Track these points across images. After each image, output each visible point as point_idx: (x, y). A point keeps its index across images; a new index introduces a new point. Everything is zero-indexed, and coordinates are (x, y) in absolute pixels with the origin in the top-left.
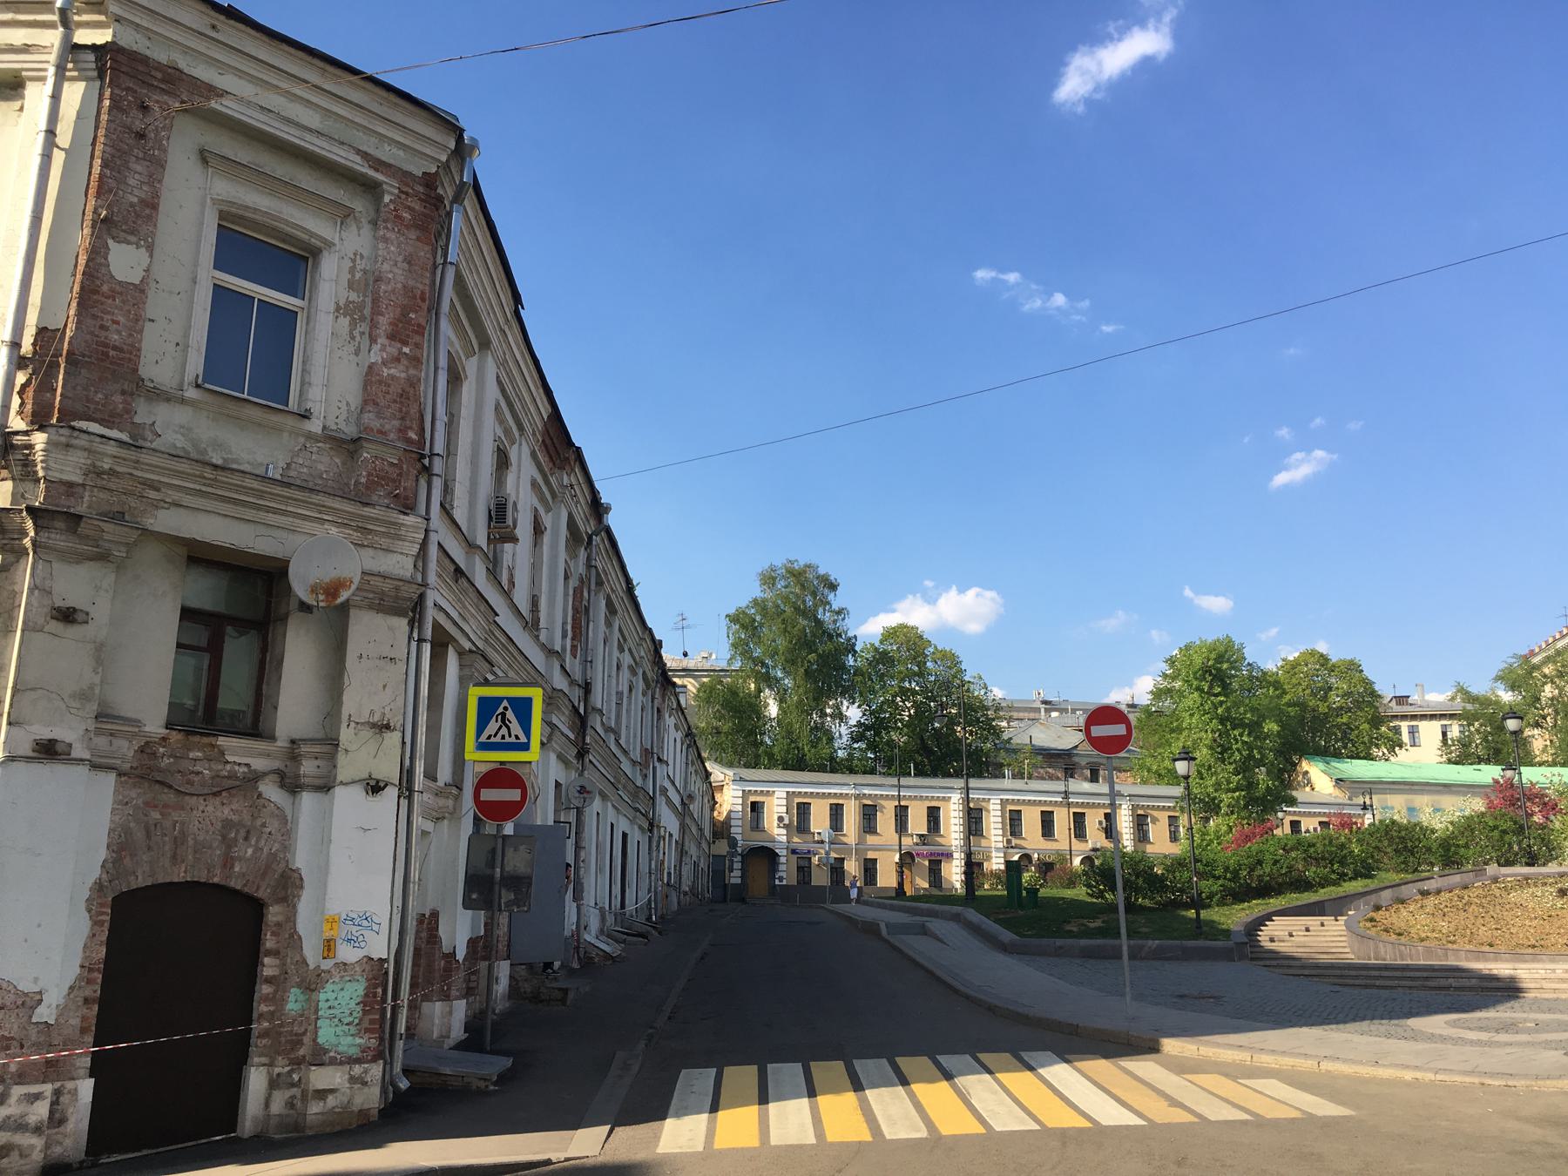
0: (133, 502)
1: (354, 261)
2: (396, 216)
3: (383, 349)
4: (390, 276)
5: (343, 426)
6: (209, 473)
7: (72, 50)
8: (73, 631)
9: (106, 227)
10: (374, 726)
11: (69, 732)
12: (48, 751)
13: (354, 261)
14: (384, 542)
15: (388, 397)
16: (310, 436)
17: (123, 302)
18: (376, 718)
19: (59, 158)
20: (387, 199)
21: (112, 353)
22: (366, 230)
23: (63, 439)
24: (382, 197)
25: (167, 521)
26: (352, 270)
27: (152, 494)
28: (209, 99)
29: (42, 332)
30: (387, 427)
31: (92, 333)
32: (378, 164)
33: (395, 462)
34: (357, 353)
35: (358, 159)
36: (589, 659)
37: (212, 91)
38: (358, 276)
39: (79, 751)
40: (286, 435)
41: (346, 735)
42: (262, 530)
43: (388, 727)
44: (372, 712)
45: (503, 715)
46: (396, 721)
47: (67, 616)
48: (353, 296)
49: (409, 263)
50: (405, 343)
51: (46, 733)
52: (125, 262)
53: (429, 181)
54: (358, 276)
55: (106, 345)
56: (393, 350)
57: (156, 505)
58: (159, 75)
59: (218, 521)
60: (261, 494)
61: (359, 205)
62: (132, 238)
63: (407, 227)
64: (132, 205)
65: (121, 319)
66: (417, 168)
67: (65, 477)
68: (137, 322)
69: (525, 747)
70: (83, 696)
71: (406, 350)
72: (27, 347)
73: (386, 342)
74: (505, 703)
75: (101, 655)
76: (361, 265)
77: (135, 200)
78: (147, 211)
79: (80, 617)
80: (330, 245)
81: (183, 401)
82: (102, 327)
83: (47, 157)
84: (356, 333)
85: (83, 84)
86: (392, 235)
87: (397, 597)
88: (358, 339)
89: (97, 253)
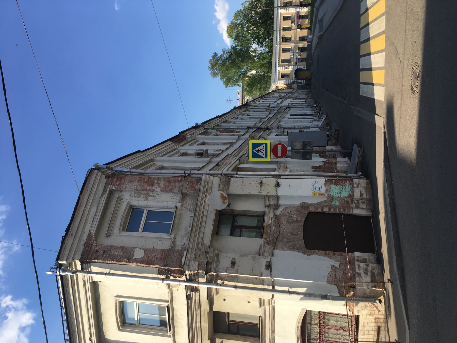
0: (203, 249)
1: (132, 196)
2: (119, 186)
3: (156, 188)
4: (135, 187)
5: (178, 197)
6: (194, 231)
7: (83, 270)
8: (237, 262)
9: (130, 259)
10: (261, 186)
11: (264, 262)
12: (268, 266)
13: (132, 196)
14: (210, 185)
15: (169, 186)
16: (182, 206)
17: (149, 254)
18: (259, 185)
19: (112, 272)
20: (114, 188)
21: (163, 256)
22: (123, 193)
23: (187, 267)
24: (114, 189)
25: (207, 241)
26: (135, 197)
27: (200, 244)
28: (92, 235)
29: (159, 273)
30: (178, 186)
31: (158, 261)
32: (104, 191)
33: (187, 183)
34: (158, 195)
35: (104, 196)
36: (240, 127)
37: (90, 234)
38: (136, 195)
39: (269, 259)
40: (182, 212)
41: (263, 193)
42: (208, 217)
43: (261, 182)
44: (257, 186)
45: (257, 151)
46: (259, 180)
47: (233, 264)
48: (142, 196)
49: (131, 182)
50: (154, 182)
51: (264, 267)
52: (139, 254)
53: (107, 177)
54: (136, 195)
55: (161, 258)
56: (156, 185)
57: (203, 243)
58: (87, 248)
59: (206, 229)
60: (199, 218)
61: (117, 195)
62: (132, 252)
63: (121, 182)
64: (123, 253)
65: (154, 254)
66: (104, 180)
67: (197, 266)
68: (154, 250)
69: (266, 145)
70: (254, 259)
71: (156, 181)
72: (163, 277)
73: (154, 187)
74: (254, 151)
75: (243, 255)
76: (133, 194)
77: (122, 252)
78: (124, 249)
79: (233, 261)
80: (128, 203)
81: (175, 238)
82: (157, 259)
83: (112, 275)
84: (152, 195)
85: (92, 267)
86: (124, 186)
87: (225, 181)
88: (154, 194)
89: (137, 261)
